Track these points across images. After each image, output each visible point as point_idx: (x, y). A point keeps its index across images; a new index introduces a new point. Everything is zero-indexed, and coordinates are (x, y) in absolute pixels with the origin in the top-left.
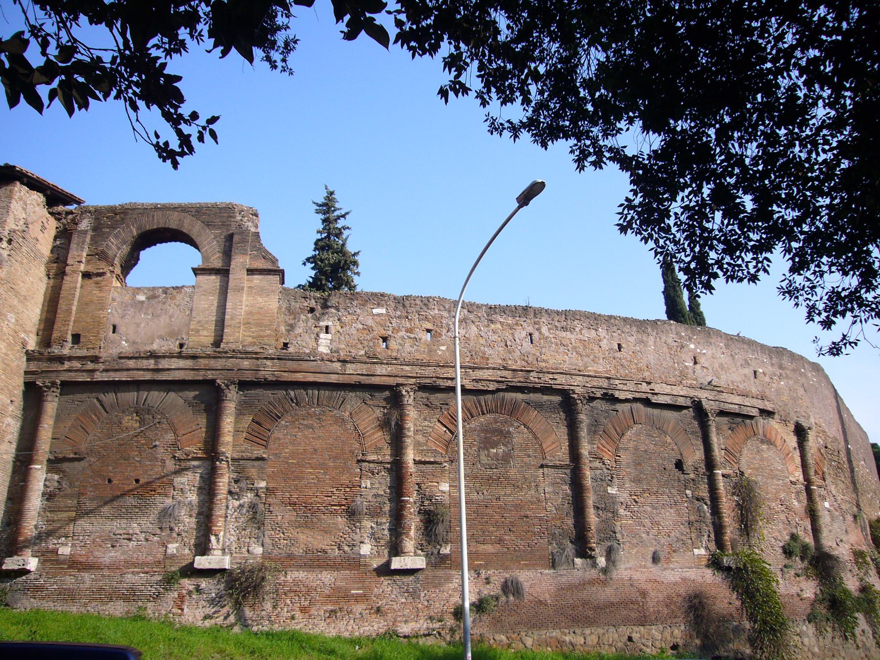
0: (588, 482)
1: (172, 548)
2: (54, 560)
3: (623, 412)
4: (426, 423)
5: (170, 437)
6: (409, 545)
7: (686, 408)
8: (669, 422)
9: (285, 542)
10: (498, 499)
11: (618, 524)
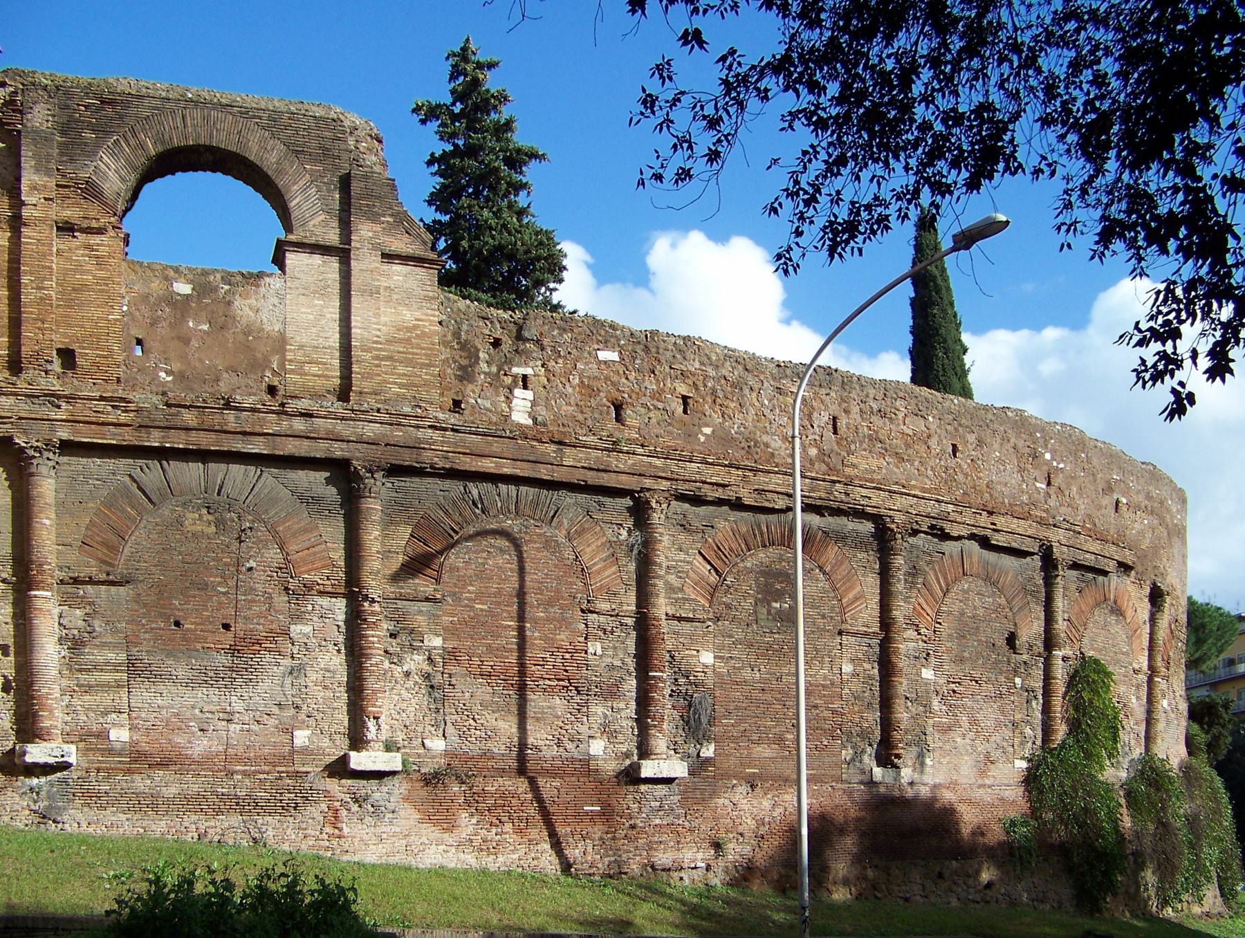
0: (902, 663)
1: (302, 737)
2: (104, 750)
3: (951, 556)
4: (682, 556)
5: (273, 555)
6: (660, 743)
7: (1033, 554)
8: (1007, 574)
9: (478, 732)
10: (779, 679)
11: (930, 721)
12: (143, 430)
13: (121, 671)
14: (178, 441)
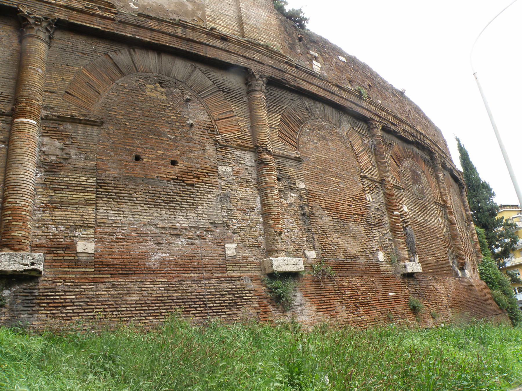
1: (231, 249)
2: (70, 261)
12: (121, 25)
13: (91, 192)
14: (146, 36)
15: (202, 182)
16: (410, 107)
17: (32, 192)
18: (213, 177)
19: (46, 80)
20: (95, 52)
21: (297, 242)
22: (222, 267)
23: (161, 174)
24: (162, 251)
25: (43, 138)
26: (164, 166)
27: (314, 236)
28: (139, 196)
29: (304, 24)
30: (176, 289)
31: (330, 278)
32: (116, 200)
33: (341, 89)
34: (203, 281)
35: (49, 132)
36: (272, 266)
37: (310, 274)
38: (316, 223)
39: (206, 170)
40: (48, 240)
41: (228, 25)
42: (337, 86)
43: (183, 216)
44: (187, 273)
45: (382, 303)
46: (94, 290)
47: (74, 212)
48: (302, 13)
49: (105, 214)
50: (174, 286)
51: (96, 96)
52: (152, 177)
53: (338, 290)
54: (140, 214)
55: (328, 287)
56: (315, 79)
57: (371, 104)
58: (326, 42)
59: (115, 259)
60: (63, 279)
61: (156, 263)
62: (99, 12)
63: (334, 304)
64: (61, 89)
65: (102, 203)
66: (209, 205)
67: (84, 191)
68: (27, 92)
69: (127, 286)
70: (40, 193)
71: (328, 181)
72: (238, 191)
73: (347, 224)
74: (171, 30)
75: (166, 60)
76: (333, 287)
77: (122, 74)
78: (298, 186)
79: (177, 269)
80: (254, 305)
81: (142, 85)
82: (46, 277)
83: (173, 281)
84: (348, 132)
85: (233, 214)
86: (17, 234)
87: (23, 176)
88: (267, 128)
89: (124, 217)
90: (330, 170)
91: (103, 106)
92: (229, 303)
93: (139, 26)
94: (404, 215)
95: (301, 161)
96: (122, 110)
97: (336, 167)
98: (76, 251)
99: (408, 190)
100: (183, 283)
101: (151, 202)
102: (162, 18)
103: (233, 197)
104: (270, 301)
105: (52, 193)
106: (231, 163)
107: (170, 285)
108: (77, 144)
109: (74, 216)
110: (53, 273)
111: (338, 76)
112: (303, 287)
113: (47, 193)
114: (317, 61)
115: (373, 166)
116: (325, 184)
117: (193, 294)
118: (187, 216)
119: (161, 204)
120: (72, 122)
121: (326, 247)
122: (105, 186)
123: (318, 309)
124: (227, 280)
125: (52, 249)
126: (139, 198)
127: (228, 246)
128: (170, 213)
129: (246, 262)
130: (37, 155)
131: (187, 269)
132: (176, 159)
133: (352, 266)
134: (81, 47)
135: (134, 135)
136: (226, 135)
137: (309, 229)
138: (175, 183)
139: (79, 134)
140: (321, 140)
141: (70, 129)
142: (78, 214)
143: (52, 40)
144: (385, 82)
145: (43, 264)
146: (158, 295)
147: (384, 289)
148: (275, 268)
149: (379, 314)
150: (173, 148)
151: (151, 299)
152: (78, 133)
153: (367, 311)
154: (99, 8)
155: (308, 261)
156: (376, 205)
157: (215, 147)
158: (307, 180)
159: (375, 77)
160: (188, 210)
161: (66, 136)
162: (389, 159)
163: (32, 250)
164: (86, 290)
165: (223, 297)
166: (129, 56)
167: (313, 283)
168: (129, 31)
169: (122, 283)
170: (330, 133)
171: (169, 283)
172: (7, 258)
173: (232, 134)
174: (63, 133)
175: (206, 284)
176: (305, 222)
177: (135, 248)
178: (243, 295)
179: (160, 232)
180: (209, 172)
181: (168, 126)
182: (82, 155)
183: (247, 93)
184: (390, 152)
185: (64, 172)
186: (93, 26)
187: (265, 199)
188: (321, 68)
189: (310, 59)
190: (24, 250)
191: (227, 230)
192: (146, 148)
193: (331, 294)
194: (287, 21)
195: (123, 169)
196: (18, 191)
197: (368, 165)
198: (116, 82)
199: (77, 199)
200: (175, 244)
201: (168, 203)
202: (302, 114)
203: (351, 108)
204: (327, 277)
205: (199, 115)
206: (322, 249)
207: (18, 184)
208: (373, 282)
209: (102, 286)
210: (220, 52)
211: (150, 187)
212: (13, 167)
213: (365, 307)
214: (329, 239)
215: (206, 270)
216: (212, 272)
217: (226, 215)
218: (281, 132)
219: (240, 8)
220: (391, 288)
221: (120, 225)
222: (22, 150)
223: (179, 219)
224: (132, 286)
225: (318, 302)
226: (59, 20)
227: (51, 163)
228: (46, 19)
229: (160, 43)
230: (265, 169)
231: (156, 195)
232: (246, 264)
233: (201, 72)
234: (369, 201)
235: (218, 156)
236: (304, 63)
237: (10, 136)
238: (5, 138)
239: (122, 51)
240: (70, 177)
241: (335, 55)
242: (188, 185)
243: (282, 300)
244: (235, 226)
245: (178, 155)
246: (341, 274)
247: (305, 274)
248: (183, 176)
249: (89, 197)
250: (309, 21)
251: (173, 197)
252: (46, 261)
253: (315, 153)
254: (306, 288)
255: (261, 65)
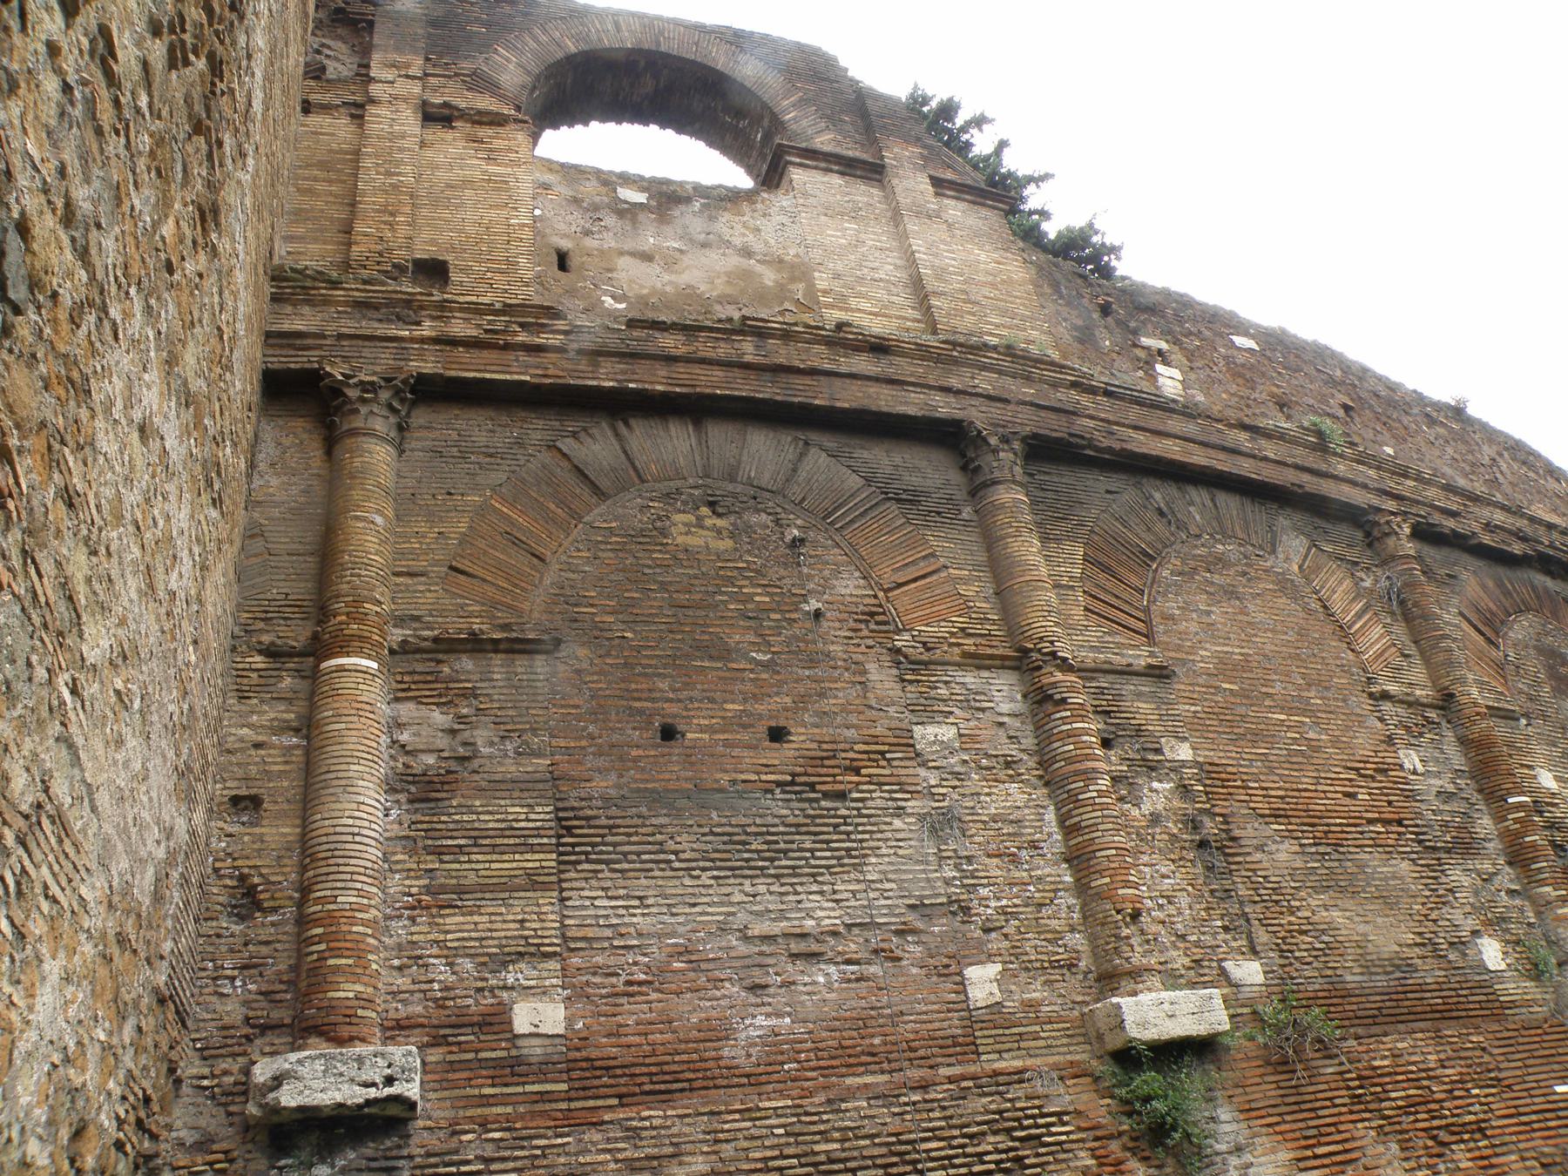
1: (983, 983)
2: (497, 1064)
13: (542, 848)
14: (658, 381)
15: (870, 783)
16: (1494, 447)
17: (376, 866)
18: (902, 764)
19: (396, 543)
20: (521, 445)
21: (1194, 938)
22: (961, 1045)
23: (742, 772)
24: (769, 1009)
25: (399, 706)
26: (749, 747)
27: (1247, 910)
28: (685, 846)
29: (1108, 264)
30: (822, 1127)
31: (1325, 1049)
32: (617, 866)
33: (1256, 433)
34: (905, 1095)
35: (413, 687)
36: (1121, 1025)
37: (1252, 1039)
38: (1247, 866)
39: (877, 744)
40: (430, 1004)
41: (886, 307)
42: (1245, 427)
43: (821, 893)
44: (854, 1075)
45: (1535, 1126)
46: (572, 1149)
47: (496, 914)
48: (1096, 233)
49: (589, 913)
50: (816, 1118)
51: (533, 567)
52: (715, 786)
53: (1361, 1087)
54: (692, 901)
55: (1323, 1079)
56: (1170, 418)
57: (1363, 463)
58: (1184, 304)
59: (629, 1046)
60: (479, 1120)
61: (753, 1051)
62: (522, 338)
63: (1353, 1139)
64: (436, 563)
65: (576, 879)
66: (901, 852)
67: (522, 848)
68: (348, 583)
69: (670, 1132)
70: (399, 867)
71: (1263, 726)
72: (982, 798)
73: (1350, 857)
74: (723, 351)
75: (720, 435)
76: (1338, 1077)
77: (600, 493)
78: (1169, 755)
79: (822, 1063)
80: (1079, 1163)
81: (659, 518)
82: (430, 1119)
83: (812, 1104)
84: (1304, 561)
85: (977, 870)
86: (341, 994)
87: (350, 822)
88: (1046, 589)
89: (643, 915)
90: (1264, 690)
91: (555, 595)
92: (997, 1162)
93: (634, 356)
94: (1548, 804)
95: (1167, 677)
96: (609, 597)
97: (1282, 678)
98: (512, 1031)
99: (1545, 717)
100: (843, 1106)
101: (721, 860)
102: (695, 320)
103: (970, 818)
104: (1131, 1145)
105: (432, 861)
106: (952, 713)
107: (803, 1118)
108: (492, 712)
109: (499, 926)
110: (448, 1103)
111: (1242, 397)
112: (1237, 1086)
113: (418, 863)
114: (1166, 363)
115: (1406, 656)
116: (1256, 737)
117: (876, 1141)
118: (835, 892)
119: (752, 864)
120: (473, 651)
121: (1293, 941)
122: (581, 827)
123: (1299, 1160)
124: (981, 1087)
125: (442, 1032)
126: (684, 852)
127: (972, 972)
128: (783, 889)
129: (1037, 1021)
130: (386, 757)
131: (852, 1060)
132: (782, 723)
133: (1394, 997)
134: (481, 438)
135: (650, 666)
136: (923, 628)
137: (1226, 891)
138: (788, 796)
139: (495, 683)
140: (1220, 602)
141: (468, 672)
142: (511, 917)
143: (407, 434)
144: (1392, 387)
145: (418, 1079)
146: (769, 1153)
147: (1530, 1070)
148: (1134, 1032)
149: (1534, 1168)
150: (769, 691)
151: (746, 1167)
152: (493, 680)
153: (1482, 1158)
154: (522, 325)
155: (1240, 996)
156: (1440, 783)
157: (895, 672)
158: (1198, 734)
159: (1360, 379)
160: (836, 873)
161: (461, 692)
162: (1456, 625)
163: (387, 1038)
164: (547, 1151)
165: (976, 1142)
166: (614, 442)
167: (1270, 1069)
168: (607, 374)
169: (656, 1122)
170: (1244, 574)
171: (799, 1111)
172: (319, 1066)
173: (943, 624)
174: (451, 685)
175: (914, 1103)
176: (1210, 869)
177: (686, 1009)
178: (1038, 1131)
179: (757, 950)
180: (886, 748)
181: (749, 628)
182: (508, 743)
183: (969, 493)
184: (1455, 601)
185: (463, 796)
186: (508, 377)
187: (1070, 810)
188: (1182, 382)
189: (1147, 363)
190: (363, 1040)
191: (963, 922)
192: (691, 699)
193: (1338, 1101)
194: (1056, 265)
195: (628, 770)
196: (338, 865)
197: (1386, 655)
198: (585, 520)
199: (502, 873)
200: (805, 985)
201: (772, 860)
202: (1149, 529)
203: (1300, 486)
204: (1311, 1043)
205: (835, 582)
206: (1282, 951)
207: (338, 846)
208: (1484, 1049)
209: (593, 1135)
210: (873, 389)
211: (714, 815)
212: (323, 799)
213: (1472, 1145)
214: (1299, 914)
215: (910, 1060)
216: (931, 1062)
217: (954, 878)
218: (1091, 595)
219: (913, 253)
220: (1556, 1067)
221: (635, 942)
222: (345, 746)
223: (812, 905)
224: (686, 1130)
225: (1298, 1134)
226: (422, 378)
227: (424, 775)
228: (388, 380)
229: (698, 390)
230: (1058, 715)
231: (736, 838)
232: (1038, 1028)
233: (824, 455)
234: (1415, 772)
235: (909, 695)
236: (1128, 377)
237: (311, 712)
238: (299, 717)
239: (594, 431)
240: (480, 809)
241: (1221, 335)
242: (826, 795)
243: (1169, 1136)
244: (988, 906)
245: (786, 709)
246: (1360, 1031)
247: (1238, 1042)
248: (810, 770)
249: (537, 864)
250: (1123, 253)
251: (786, 838)
252: (427, 1068)
253: (1208, 646)
254: (1247, 1089)
255: (999, 405)
